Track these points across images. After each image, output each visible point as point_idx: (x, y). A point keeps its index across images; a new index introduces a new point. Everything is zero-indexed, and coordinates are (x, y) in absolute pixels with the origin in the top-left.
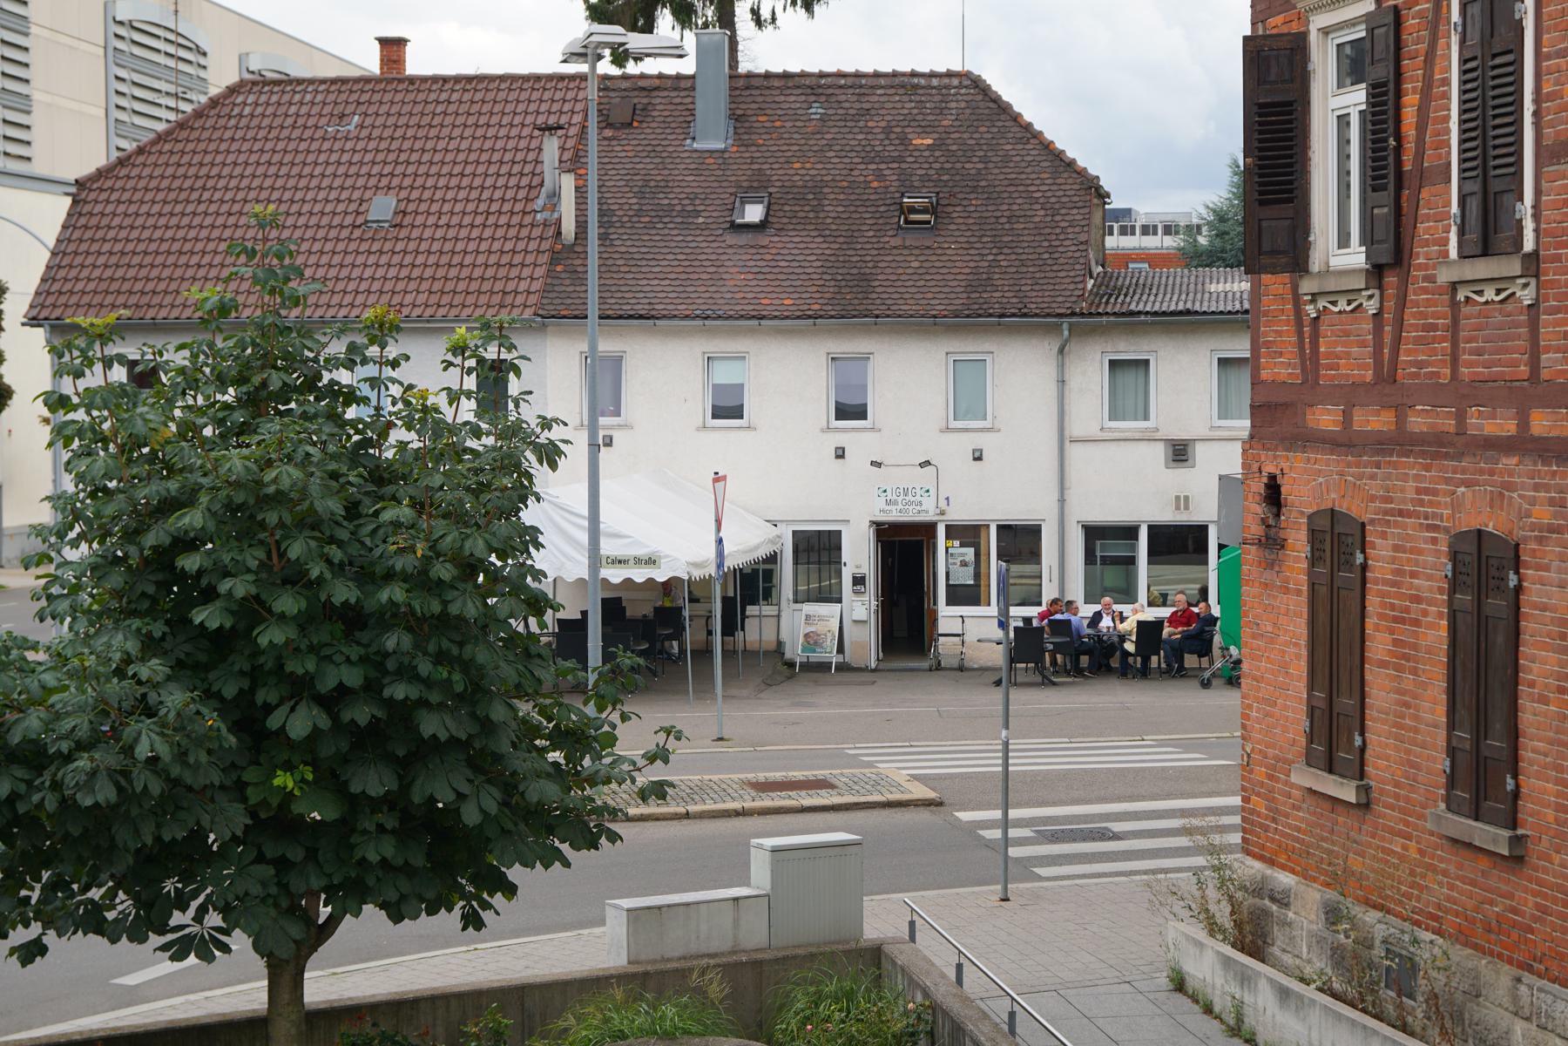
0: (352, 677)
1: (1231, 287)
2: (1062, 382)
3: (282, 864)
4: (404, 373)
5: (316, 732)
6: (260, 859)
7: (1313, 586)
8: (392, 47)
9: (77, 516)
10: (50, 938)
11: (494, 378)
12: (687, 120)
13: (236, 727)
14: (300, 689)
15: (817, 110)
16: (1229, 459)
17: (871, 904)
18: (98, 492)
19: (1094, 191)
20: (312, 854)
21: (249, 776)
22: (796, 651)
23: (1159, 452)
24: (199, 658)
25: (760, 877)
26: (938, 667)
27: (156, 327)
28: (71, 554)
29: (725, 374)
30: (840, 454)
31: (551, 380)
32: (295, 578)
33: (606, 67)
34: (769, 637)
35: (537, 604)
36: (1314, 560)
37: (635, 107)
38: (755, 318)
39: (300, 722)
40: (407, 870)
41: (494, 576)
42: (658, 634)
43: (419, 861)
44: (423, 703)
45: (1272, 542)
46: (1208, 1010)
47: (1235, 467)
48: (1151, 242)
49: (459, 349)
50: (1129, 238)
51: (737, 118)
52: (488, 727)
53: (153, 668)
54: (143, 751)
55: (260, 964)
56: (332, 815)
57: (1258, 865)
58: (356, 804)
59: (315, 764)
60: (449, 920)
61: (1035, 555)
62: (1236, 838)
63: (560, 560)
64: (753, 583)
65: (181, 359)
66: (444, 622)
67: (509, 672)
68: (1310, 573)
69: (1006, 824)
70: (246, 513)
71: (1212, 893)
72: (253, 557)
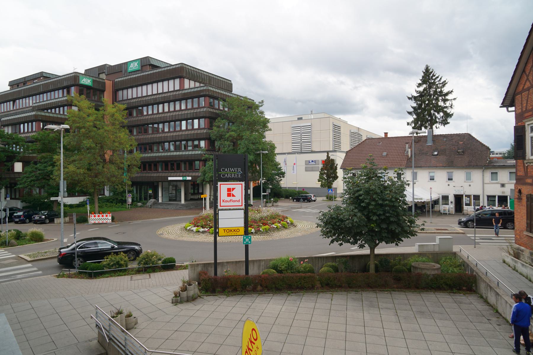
0: (381, 213)
1: (513, 162)
2: (483, 175)
3: (372, 236)
4: (388, 175)
5: (377, 219)
6: (369, 235)
7: (527, 205)
8: (386, 134)
9: (347, 192)
10: (343, 243)
11: (399, 175)
12: (426, 141)
13: (366, 218)
14: (375, 214)
15: (445, 139)
16: (512, 187)
17: (454, 246)
18: (349, 189)
19: (488, 149)
20: (376, 235)
21: (368, 224)
22: (442, 211)
23: (499, 185)
24: (362, 209)
25: (438, 242)
26: (464, 214)
27: (356, 169)
28: (346, 196)
29: (432, 174)
30: (449, 185)
31: (407, 175)
32: (374, 200)
33: (415, 135)
34: (438, 209)
35: (406, 204)
36: (527, 201)
37: (419, 140)
38: (436, 167)
39: (375, 218)
40: (388, 237)
41: (400, 200)
42: (422, 208)
43: (390, 236)
44: (391, 216)
45: (520, 199)
46: (509, 266)
47: (513, 188)
48: (497, 156)
49: (396, 172)
50: (226, 192)
51: (433, 141)
52: (399, 220)
53: (356, 211)
54: (355, 220)
55: (369, 248)
56: (379, 230)
57: (518, 246)
58: (382, 229)
59: (376, 223)
60: (394, 244)
61: (479, 199)
62: (514, 241)
63: (409, 199)
64: (436, 202)
65: (360, 173)
66: (394, 206)
67: (402, 213)
68: (527, 203)
69: (475, 237)
70: (368, 192)
71: (510, 249)
72: (369, 197)
